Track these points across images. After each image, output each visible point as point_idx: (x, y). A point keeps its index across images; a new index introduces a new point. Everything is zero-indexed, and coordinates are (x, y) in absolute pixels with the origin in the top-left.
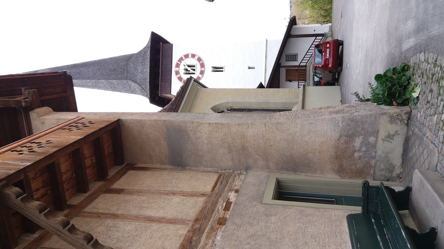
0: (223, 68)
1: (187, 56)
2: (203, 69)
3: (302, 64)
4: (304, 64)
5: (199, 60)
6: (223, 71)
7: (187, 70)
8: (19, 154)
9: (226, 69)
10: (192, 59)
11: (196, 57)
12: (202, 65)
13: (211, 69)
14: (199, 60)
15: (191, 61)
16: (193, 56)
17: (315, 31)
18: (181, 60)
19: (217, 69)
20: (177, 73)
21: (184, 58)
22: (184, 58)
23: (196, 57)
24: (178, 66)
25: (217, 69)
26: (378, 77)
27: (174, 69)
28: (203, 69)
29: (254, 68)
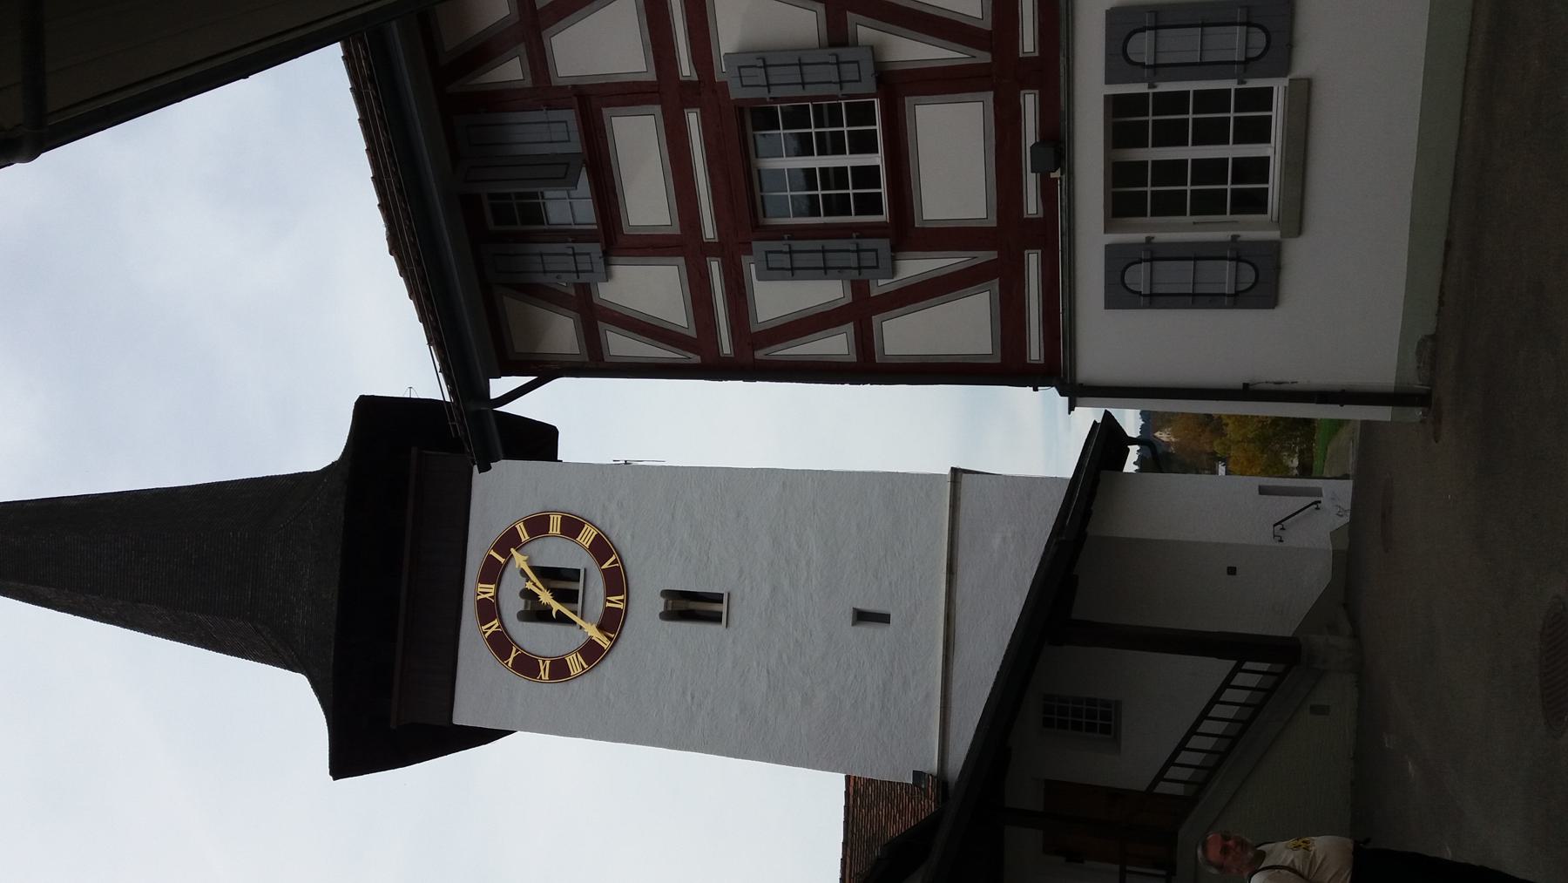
0: (717, 598)
1: (538, 525)
2: (616, 602)
3: (1163, 788)
4: (1178, 789)
5: (601, 548)
6: (715, 618)
7: (561, 596)
8: (1263, 491)
9: (738, 611)
10: (566, 544)
11: (587, 536)
12: (616, 582)
13: (660, 605)
14: (601, 548)
15: (558, 552)
16: (572, 527)
17: (1232, 571)
18: (508, 542)
19: (690, 607)
20: (488, 610)
21: (524, 536)
22: (524, 536)
23: (587, 536)
24: (492, 572)
25: (690, 607)
26: (1036, 390)
27: (475, 590)
28: (616, 602)
29: (883, 618)
